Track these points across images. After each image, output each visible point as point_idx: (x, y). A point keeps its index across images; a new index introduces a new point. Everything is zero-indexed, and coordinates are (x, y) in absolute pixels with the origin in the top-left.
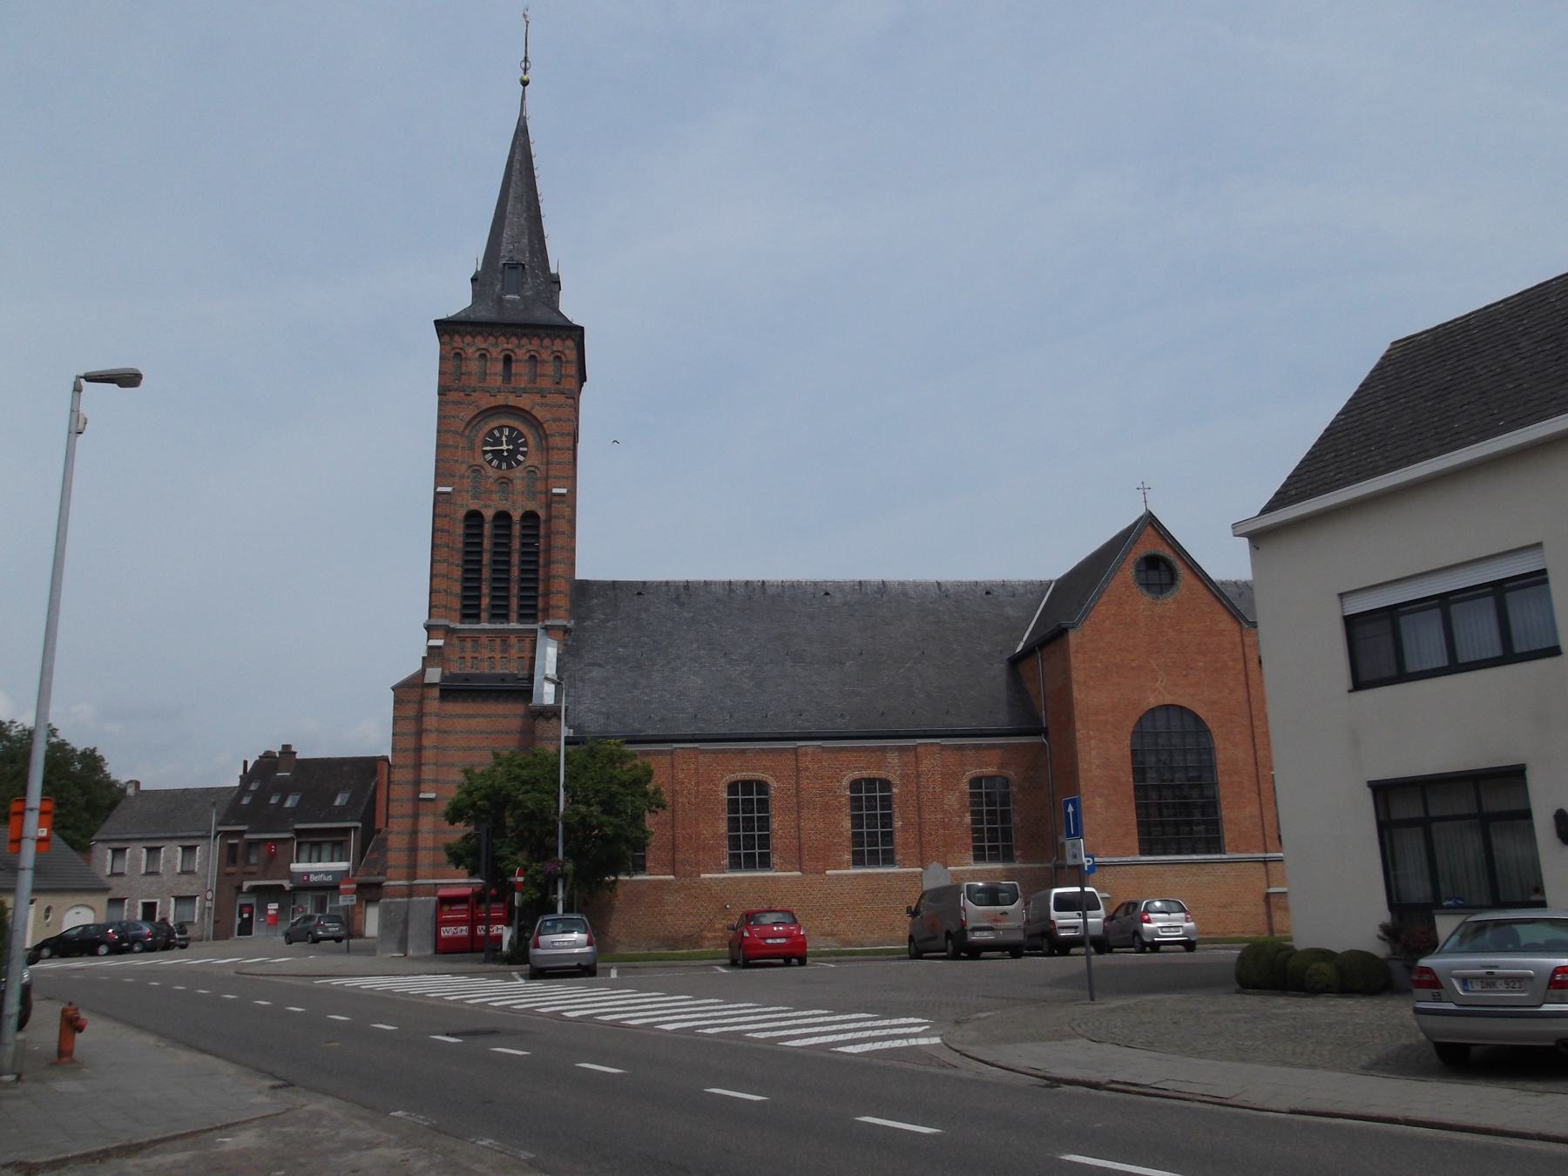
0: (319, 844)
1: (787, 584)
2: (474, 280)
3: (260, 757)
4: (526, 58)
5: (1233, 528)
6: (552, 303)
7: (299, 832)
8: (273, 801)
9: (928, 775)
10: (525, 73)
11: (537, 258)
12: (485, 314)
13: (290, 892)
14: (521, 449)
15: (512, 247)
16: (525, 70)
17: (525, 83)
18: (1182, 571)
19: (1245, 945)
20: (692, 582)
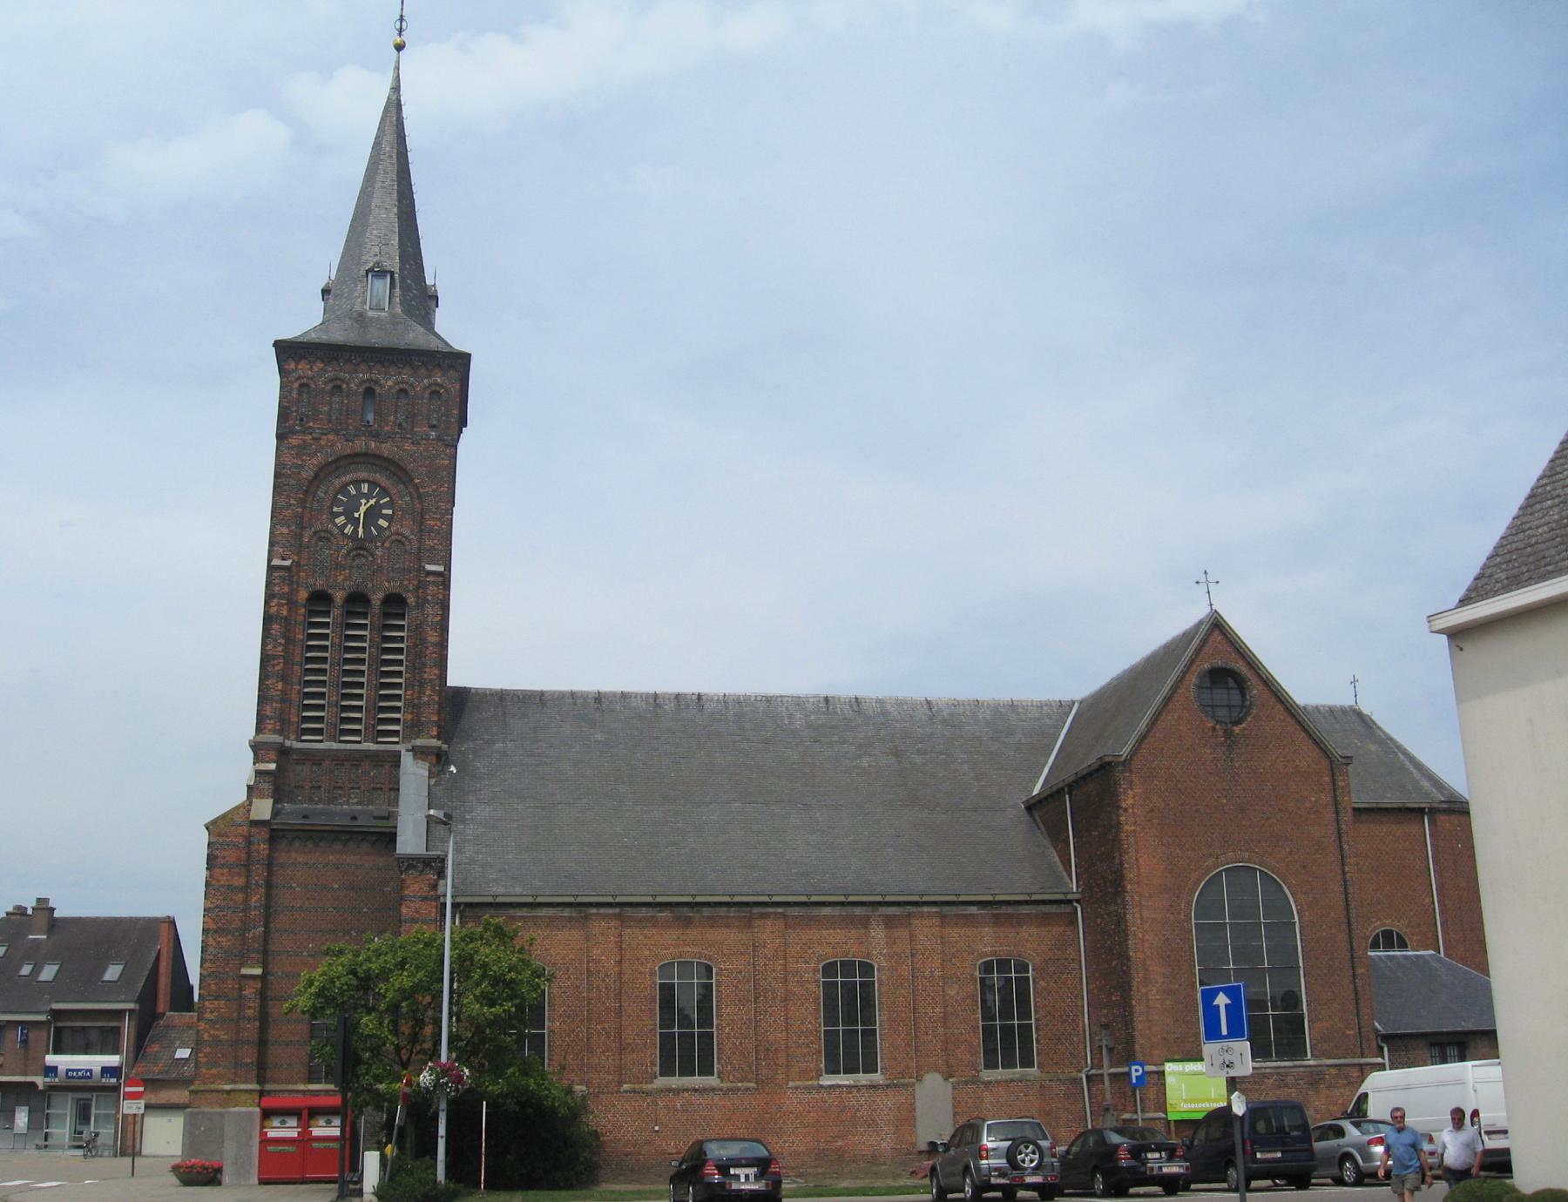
0: (322, 839)
1: (731, 699)
2: (326, 292)
3: (8, 914)
4: (402, 16)
5: (1429, 622)
6: (427, 322)
7: (56, 1014)
8: (26, 970)
9: (923, 954)
10: (400, 35)
11: (410, 265)
12: (338, 335)
13: (43, 1092)
14: (384, 511)
15: (378, 250)
16: (400, 31)
17: (400, 47)
18: (1256, 691)
19: (1316, 1173)
20: (605, 693)
